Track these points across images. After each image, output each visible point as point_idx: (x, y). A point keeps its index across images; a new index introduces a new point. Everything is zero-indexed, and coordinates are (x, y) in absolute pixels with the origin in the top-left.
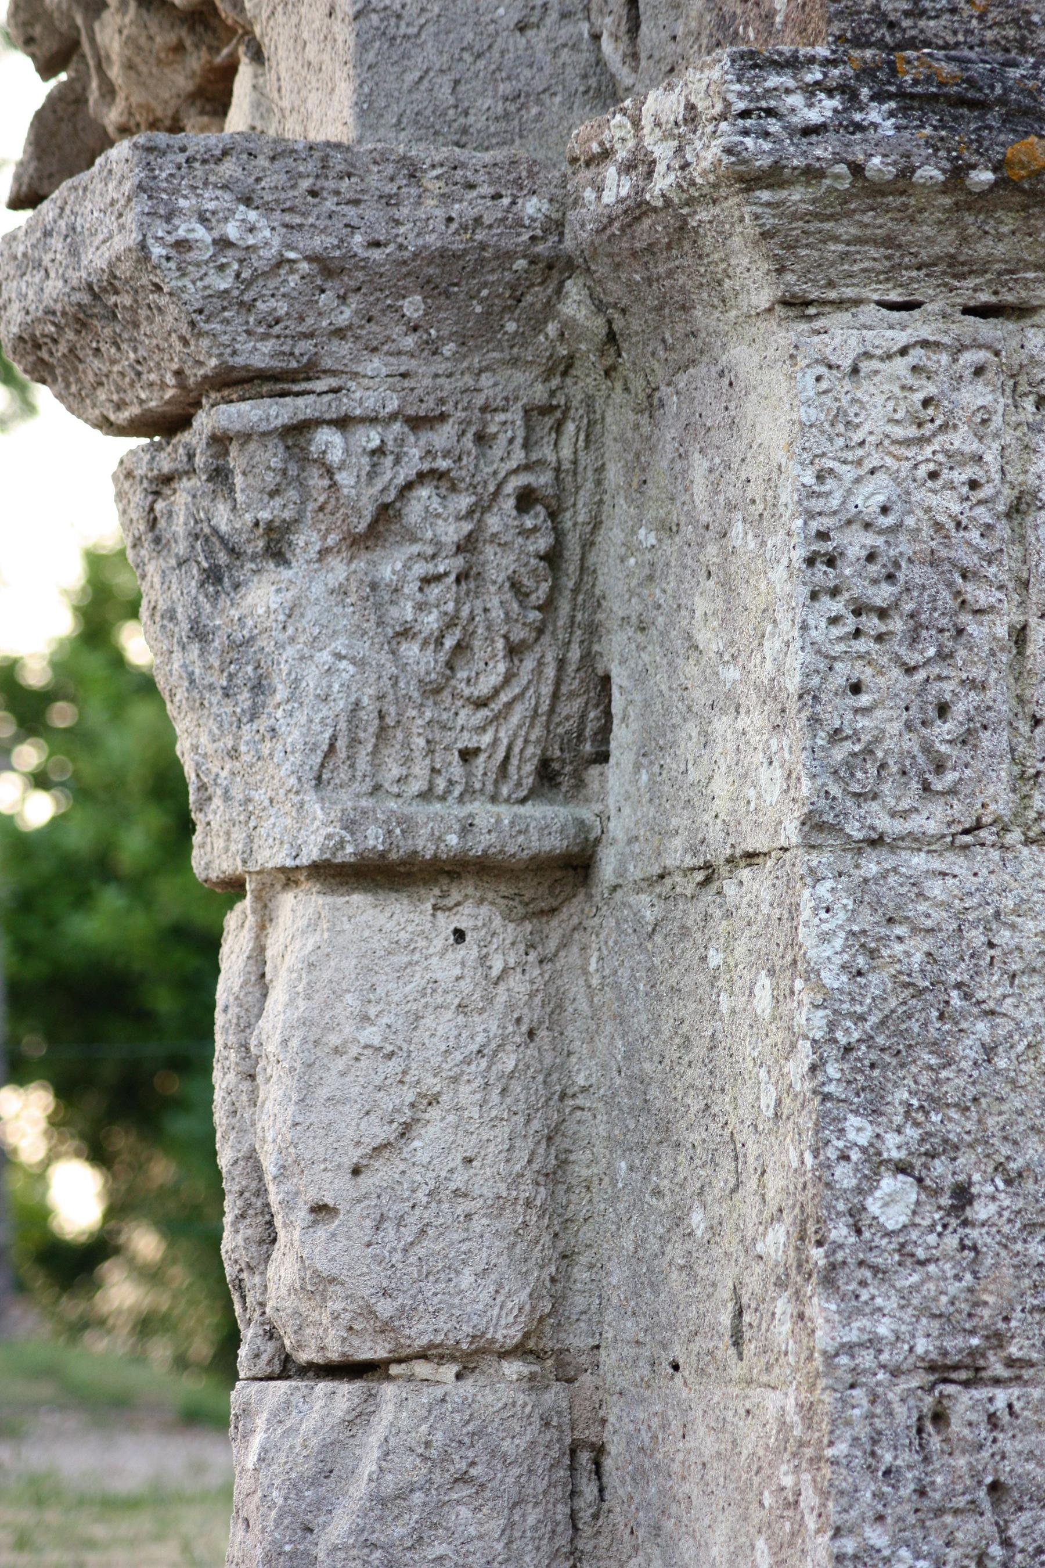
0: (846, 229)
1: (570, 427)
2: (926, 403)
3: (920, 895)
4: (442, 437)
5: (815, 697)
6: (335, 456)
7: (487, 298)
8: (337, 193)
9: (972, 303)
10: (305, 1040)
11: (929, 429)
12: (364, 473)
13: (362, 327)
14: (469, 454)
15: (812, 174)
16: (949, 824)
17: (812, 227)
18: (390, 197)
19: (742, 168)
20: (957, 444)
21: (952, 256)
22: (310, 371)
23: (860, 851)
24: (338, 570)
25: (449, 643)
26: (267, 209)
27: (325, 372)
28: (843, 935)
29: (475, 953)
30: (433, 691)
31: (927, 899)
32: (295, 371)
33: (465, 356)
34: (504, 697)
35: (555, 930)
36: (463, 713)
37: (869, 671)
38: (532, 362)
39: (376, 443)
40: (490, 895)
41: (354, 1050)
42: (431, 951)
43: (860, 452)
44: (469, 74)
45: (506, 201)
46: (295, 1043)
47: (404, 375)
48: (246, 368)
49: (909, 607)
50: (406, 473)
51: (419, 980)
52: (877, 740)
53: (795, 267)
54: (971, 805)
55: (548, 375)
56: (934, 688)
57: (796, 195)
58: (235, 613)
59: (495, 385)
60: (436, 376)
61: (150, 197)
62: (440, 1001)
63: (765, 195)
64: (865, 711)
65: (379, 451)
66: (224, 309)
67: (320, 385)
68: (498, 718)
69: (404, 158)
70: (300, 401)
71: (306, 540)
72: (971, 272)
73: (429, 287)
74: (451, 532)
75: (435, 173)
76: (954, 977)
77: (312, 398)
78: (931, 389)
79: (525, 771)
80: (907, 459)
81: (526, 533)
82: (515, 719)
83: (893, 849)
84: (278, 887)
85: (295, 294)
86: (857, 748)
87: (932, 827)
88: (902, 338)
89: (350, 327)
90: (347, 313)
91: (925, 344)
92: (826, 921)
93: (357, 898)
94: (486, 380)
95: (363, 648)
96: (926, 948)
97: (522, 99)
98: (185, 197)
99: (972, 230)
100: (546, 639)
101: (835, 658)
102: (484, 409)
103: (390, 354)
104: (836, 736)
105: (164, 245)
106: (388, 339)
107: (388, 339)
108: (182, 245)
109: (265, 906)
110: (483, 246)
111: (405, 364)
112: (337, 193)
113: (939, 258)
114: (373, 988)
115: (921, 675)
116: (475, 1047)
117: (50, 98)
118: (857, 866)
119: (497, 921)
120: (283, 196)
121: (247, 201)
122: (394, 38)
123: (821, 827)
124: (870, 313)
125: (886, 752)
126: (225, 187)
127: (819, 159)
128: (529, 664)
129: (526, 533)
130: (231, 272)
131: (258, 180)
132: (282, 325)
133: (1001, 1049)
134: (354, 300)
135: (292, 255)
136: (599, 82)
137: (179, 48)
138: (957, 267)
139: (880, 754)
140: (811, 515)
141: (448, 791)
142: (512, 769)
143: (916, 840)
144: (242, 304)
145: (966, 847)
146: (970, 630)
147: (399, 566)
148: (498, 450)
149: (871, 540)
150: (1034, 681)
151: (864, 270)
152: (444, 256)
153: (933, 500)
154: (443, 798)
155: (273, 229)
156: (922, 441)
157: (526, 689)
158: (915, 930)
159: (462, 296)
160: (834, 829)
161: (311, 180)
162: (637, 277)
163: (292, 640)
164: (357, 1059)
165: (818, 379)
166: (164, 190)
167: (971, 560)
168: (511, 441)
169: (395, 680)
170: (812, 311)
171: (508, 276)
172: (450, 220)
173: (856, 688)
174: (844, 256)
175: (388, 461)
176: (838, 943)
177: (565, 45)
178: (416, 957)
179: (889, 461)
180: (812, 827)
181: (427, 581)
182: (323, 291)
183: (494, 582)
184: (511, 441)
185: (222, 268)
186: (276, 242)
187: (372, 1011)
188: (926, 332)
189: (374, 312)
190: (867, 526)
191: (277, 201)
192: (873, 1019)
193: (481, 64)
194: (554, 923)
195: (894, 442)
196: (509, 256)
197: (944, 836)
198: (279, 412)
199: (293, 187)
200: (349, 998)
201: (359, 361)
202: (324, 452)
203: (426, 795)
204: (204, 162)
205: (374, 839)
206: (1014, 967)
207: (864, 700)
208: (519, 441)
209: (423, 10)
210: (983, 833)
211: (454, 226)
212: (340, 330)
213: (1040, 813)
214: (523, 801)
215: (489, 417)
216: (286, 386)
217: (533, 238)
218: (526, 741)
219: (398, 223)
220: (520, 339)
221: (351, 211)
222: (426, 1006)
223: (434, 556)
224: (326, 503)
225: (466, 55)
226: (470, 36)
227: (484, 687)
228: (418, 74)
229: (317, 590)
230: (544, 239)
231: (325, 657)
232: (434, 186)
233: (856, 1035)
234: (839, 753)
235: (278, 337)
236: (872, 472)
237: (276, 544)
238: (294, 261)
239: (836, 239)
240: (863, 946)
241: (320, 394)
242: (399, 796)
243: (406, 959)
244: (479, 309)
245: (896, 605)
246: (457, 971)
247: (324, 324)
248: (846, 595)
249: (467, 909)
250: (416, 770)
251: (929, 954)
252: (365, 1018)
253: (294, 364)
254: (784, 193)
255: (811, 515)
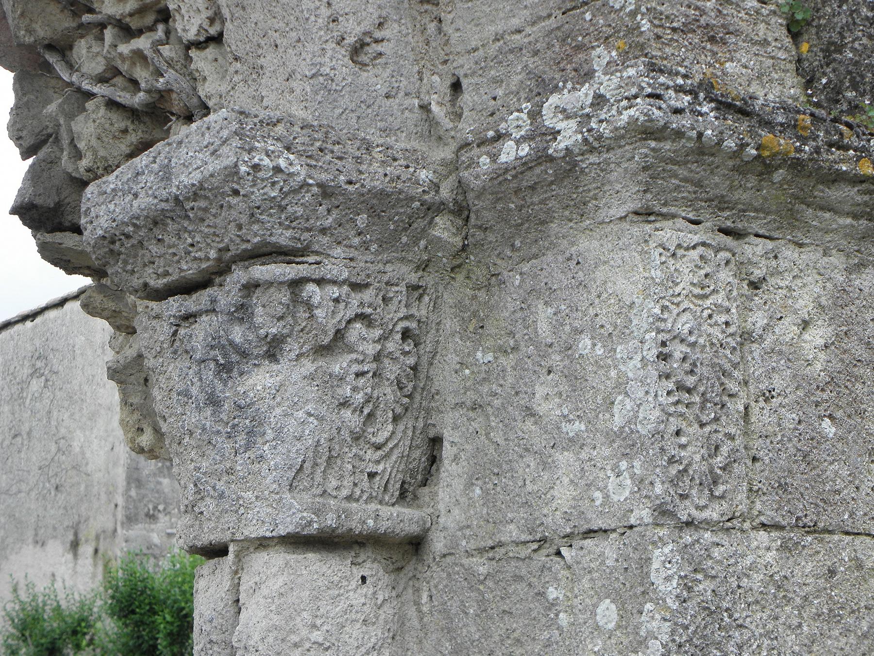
0: (682, 172)
1: (426, 299)
2: (706, 275)
3: (708, 556)
4: (368, 295)
5: (662, 436)
6: (316, 300)
7: (396, 222)
8: (332, 152)
9: (723, 226)
10: (276, 639)
11: (707, 291)
12: (330, 311)
13: (335, 229)
14: (380, 306)
15: (679, 134)
16: (722, 515)
17: (669, 167)
18: (358, 158)
19: (648, 124)
20: (720, 301)
21: (723, 196)
22: (305, 251)
23: (681, 529)
24: (308, 366)
25: (366, 411)
26: (300, 154)
27: (312, 252)
28: (676, 577)
29: (371, 591)
30: (356, 438)
31: (711, 558)
32: (298, 250)
33: (380, 254)
34: (390, 445)
35: (403, 577)
36: (369, 452)
37: (684, 423)
38: (411, 261)
39: (336, 295)
40: (379, 557)
41: (307, 645)
42: (350, 588)
43: (679, 299)
44: (364, 115)
45: (411, 170)
46: (270, 640)
47: (351, 259)
48: (274, 245)
49: (702, 389)
50: (350, 314)
51: (342, 605)
52: (690, 464)
53: (654, 190)
54: (732, 505)
55: (418, 268)
56: (714, 436)
57: (667, 145)
58: (241, 389)
59: (394, 271)
60: (366, 262)
61: (240, 139)
62: (354, 617)
63: (653, 144)
64: (683, 447)
65: (337, 300)
66: (271, 208)
67: (311, 259)
68: (387, 456)
69: (364, 139)
70: (300, 267)
71: (292, 347)
72: (727, 208)
73: (373, 213)
74: (371, 349)
75: (378, 149)
76: (725, 605)
77: (306, 265)
78: (708, 270)
79: (395, 488)
80: (700, 306)
81: (406, 354)
82: (394, 458)
83: (697, 528)
84: (252, 550)
85: (307, 204)
86: (681, 468)
87: (715, 516)
88: (696, 239)
89: (330, 228)
90: (330, 220)
91: (704, 244)
92: (669, 569)
93: (310, 555)
94: (389, 268)
95: (323, 410)
96: (712, 587)
97: (388, 132)
98: (258, 141)
99: (736, 183)
100: (409, 414)
101: (670, 415)
102: (387, 283)
103: (346, 246)
104: (672, 461)
105: (248, 166)
106: (347, 238)
107: (347, 238)
108: (256, 167)
109: (240, 560)
110: (400, 192)
111: (353, 253)
112: (332, 152)
113: (717, 197)
114: (318, 609)
115: (708, 429)
116: (371, 645)
117: (31, 166)
118: (681, 537)
119: (381, 572)
120: (308, 149)
121: (288, 149)
122: (330, 90)
123: (664, 513)
124: (680, 223)
125: (694, 471)
126: (278, 139)
127: (683, 126)
128: (401, 427)
129: (406, 354)
130: (278, 187)
131: (295, 138)
132: (298, 222)
133: (745, 647)
134: (335, 213)
135: (311, 181)
136: (422, 129)
137: (125, 131)
138: (721, 204)
139: (691, 472)
140: (659, 331)
141: (360, 497)
142: (390, 486)
143: (708, 523)
144: (280, 206)
145: (728, 529)
146: (729, 405)
147: (345, 365)
148: (392, 307)
149: (685, 348)
150: (755, 437)
151: (683, 198)
152: (382, 194)
153: (710, 330)
154: (357, 500)
155: (302, 166)
156: (705, 297)
157: (400, 441)
158: (706, 576)
159: (385, 219)
160: (672, 514)
161: (320, 143)
162: (512, 206)
163: (279, 404)
164: (308, 650)
165: (661, 254)
166: (248, 136)
167: (727, 366)
168: (400, 302)
169: (339, 429)
170: (652, 218)
171: (409, 210)
172: (386, 175)
173: (678, 433)
174: (677, 188)
175: (342, 305)
176: (675, 583)
177: (407, 109)
178: (342, 592)
179: (692, 306)
180: (660, 513)
181: (358, 375)
182: (320, 205)
183: (388, 379)
184: (400, 302)
185: (273, 184)
186: (303, 173)
187: (319, 622)
188: (704, 238)
189: (343, 221)
190: (682, 341)
191: (304, 151)
192: (692, 628)
193: (369, 111)
194: (402, 575)
195: (693, 296)
196: (412, 199)
197: (720, 522)
198: (290, 271)
199: (312, 145)
200: (305, 614)
201: (331, 248)
202: (310, 297)
203: (349, 498)
204: (268, 124)
205: (330, 520)
206: (750, 600)
207: (683, 440)
208: (404, 302)
209: (344, 79)
210: (735, 522)
211: (388, 179)
212: (324, 229)
213: (760, 512)
214: (393, 505)
215: (389, 288)
216: (292, 258)
217: (424, 191)
218: (398, 471)
219: (361, 172)
220: (406, 247)
221: (339, 163)
222: (347, 620)
223: (363, 361)
224: (305, 327)
225: (362, 105)
226: (365, 96)
227: (380, 439)
228: (341, 110)
229: (295, 376)
230: (428, 193)
231: (301, 414)
232: (379, 157)
233: (684, 638)
234: (673, 470)
235: (294, 228)
236: (683, 311)
237: (273, 349)
238: (311, 185)
239: (676, 176)
240: (685, 584)
241: (310, 264)
242: (336, 497)
243: (337, 592)
244: (392, 227)
245: (695, 388)
246: (363, 600)
247: (318, 224)
248: (674, 379)
249: (368, 565)
250: (345, 483)
251: (714, 591)
252: (314, 626)
253: (299, 246)
254: (662, 144)
255: (659, 331)
